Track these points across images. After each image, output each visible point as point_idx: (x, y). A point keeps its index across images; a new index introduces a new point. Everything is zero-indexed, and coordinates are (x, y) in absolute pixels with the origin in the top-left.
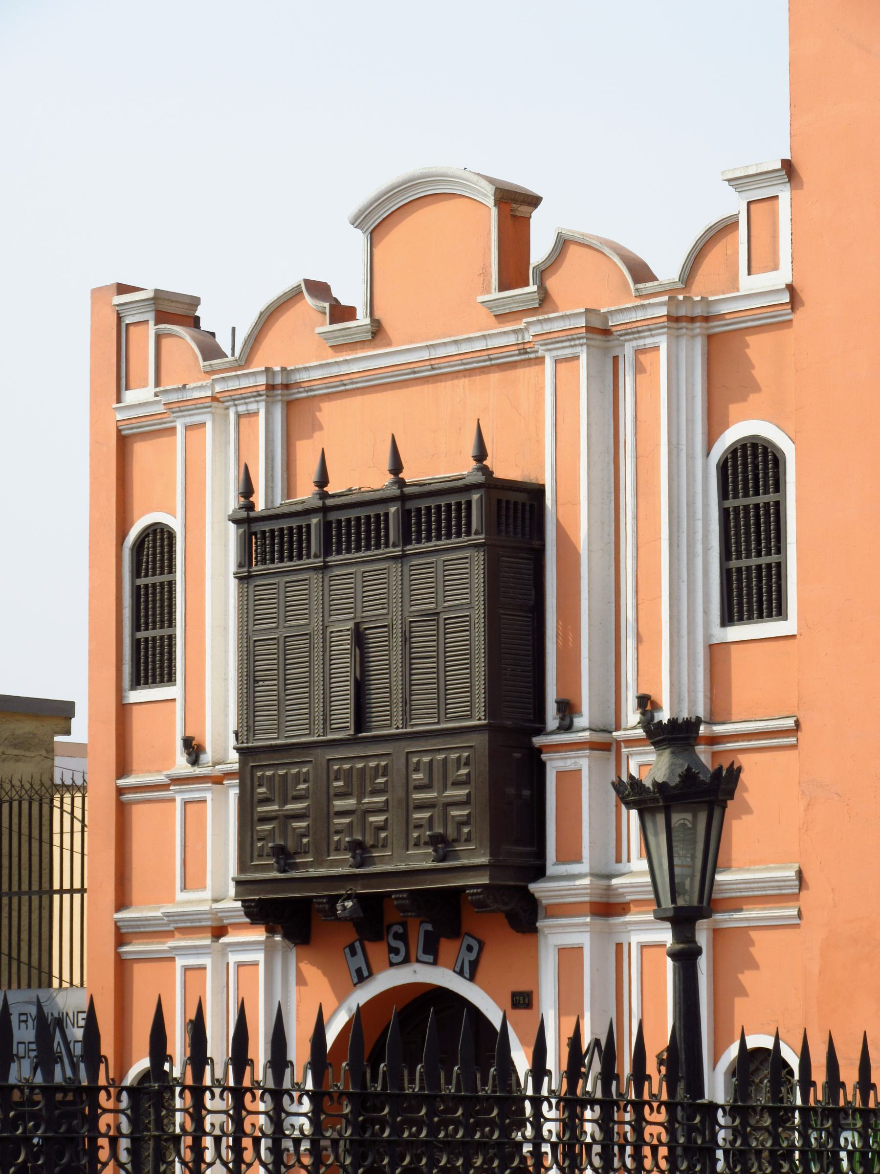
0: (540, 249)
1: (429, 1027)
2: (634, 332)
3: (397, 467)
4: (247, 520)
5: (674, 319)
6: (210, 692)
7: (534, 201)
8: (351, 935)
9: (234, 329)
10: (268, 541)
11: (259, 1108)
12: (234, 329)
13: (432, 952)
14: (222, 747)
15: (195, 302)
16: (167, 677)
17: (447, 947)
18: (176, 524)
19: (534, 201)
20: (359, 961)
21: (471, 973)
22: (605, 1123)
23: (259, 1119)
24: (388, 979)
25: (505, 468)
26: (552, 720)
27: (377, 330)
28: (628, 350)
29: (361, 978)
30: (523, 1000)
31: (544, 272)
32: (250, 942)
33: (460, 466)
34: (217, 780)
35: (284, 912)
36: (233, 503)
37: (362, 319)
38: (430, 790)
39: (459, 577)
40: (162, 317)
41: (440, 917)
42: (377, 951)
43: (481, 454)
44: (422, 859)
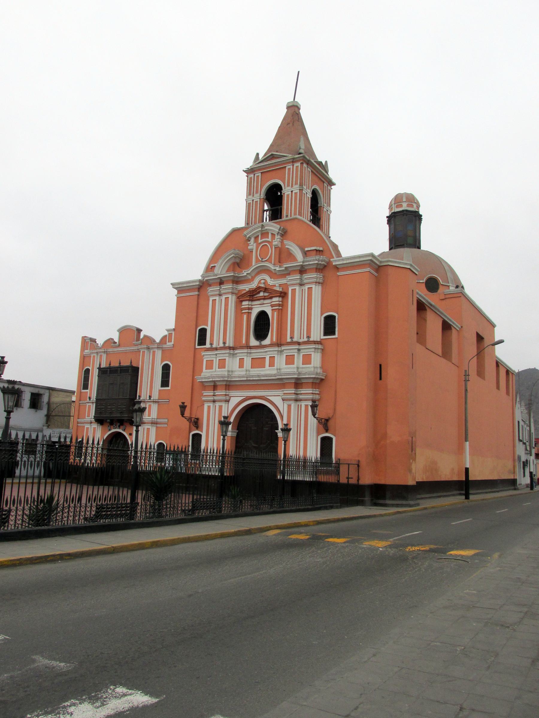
0: (142, 337)
1: (117, 438)
2: (153, 348)
3: (120, 364)
4: (100, 369)
5: (316, 269)
6: (93, 391)
7: (141, 330)
8: (109, 424)
9: (299, 72)
10: (102, 371)
11: (95, 449)
12: (299, 72)
13: (119, 427)
14: (94, 398)
15: (96, 340)
16: (87, 389)
17: (121, 427)
18: (90, 368)
19: (141, 330)
20: (109, 428)
21: (124, 430)
22: (145, 454)
23: (95, 451)
24: (113, 430)
25: (134, 365)
26: (138, 398)
27: (119, 346)
28: (152, 351)
29: (110, 430)
30: (131, 434)
31: (142, 339)
32: (95, 425)
33: (128, 364)
34: (93, 403)
35: (100, 420)
36: (98, 366)
37: (118, 343)
38: (200, 422)
39: (128, 378)
40: (91, 341)
41: (121, 423)
42: (112, 427)
43: (131, 363)
44: (118, 415)
